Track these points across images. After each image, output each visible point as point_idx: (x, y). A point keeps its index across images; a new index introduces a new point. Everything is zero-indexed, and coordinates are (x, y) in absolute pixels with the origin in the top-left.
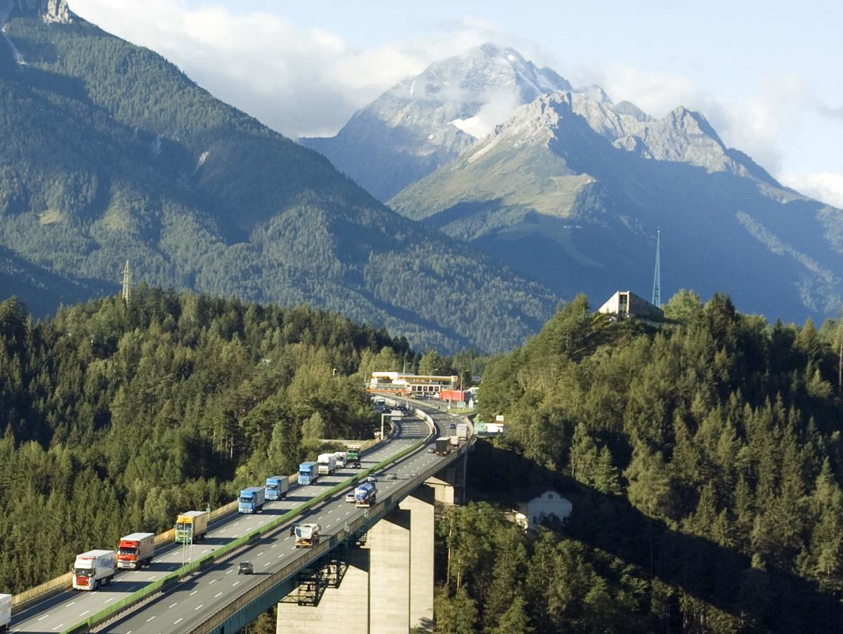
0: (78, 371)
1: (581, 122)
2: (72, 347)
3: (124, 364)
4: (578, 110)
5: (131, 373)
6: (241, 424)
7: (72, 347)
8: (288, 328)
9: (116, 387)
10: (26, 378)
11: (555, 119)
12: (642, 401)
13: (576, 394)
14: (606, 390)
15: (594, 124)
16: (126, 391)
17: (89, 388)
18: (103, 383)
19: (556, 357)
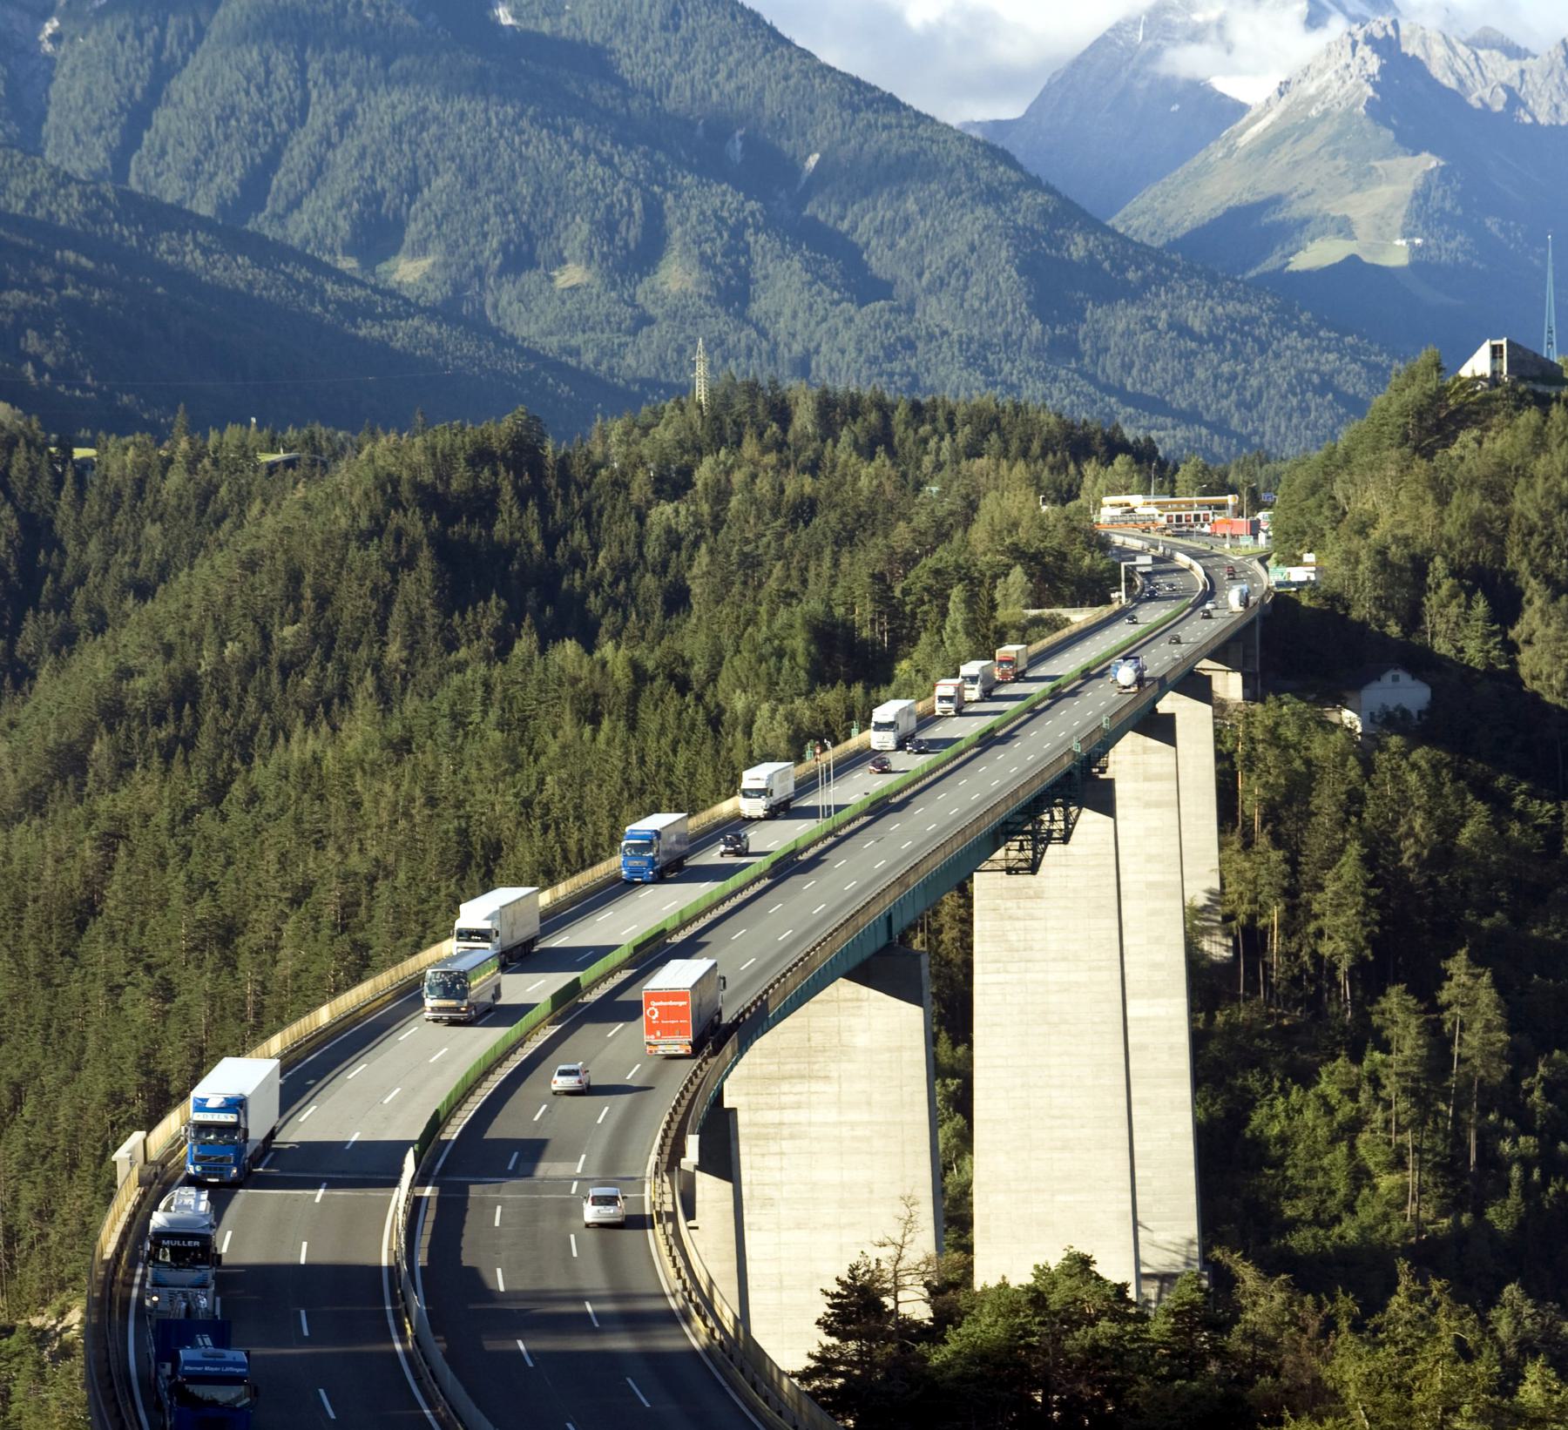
0: (632, 523)
1: (1416, 67)
2: (620, 484)
3: (705, 508)
4: (1411, 48)
5: (718, 522)
6: (897, 593)
7: (620, 484)
8: (964, 434)
9: (695, 545)
10: (551, 538)
11: (1374, 64)
12: (1534, 516)
13: (1429, 511)
14: (1476, 502)
15: (1438, 71)
16: (711, 551)
17: (652, 551)
18: (673, 541)
19: (1394, 454)
